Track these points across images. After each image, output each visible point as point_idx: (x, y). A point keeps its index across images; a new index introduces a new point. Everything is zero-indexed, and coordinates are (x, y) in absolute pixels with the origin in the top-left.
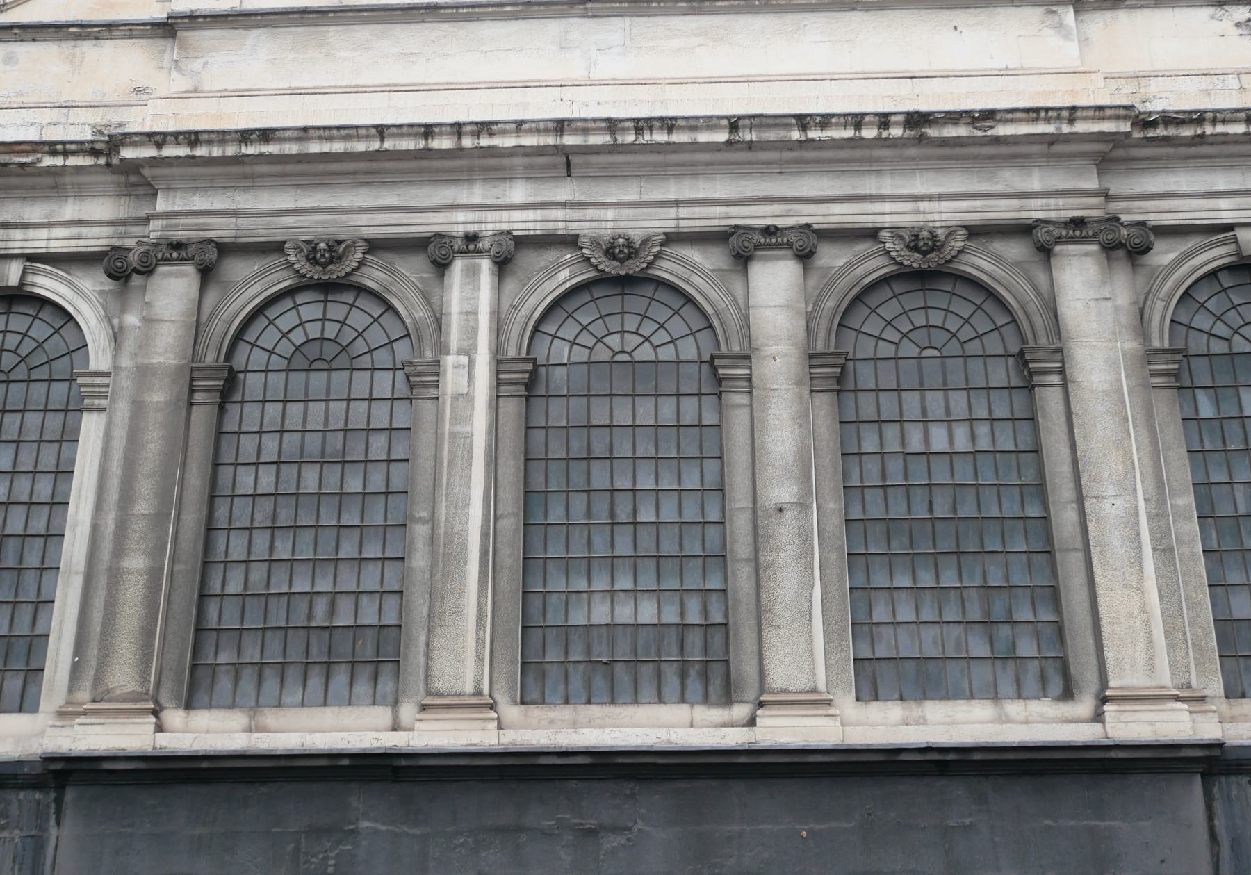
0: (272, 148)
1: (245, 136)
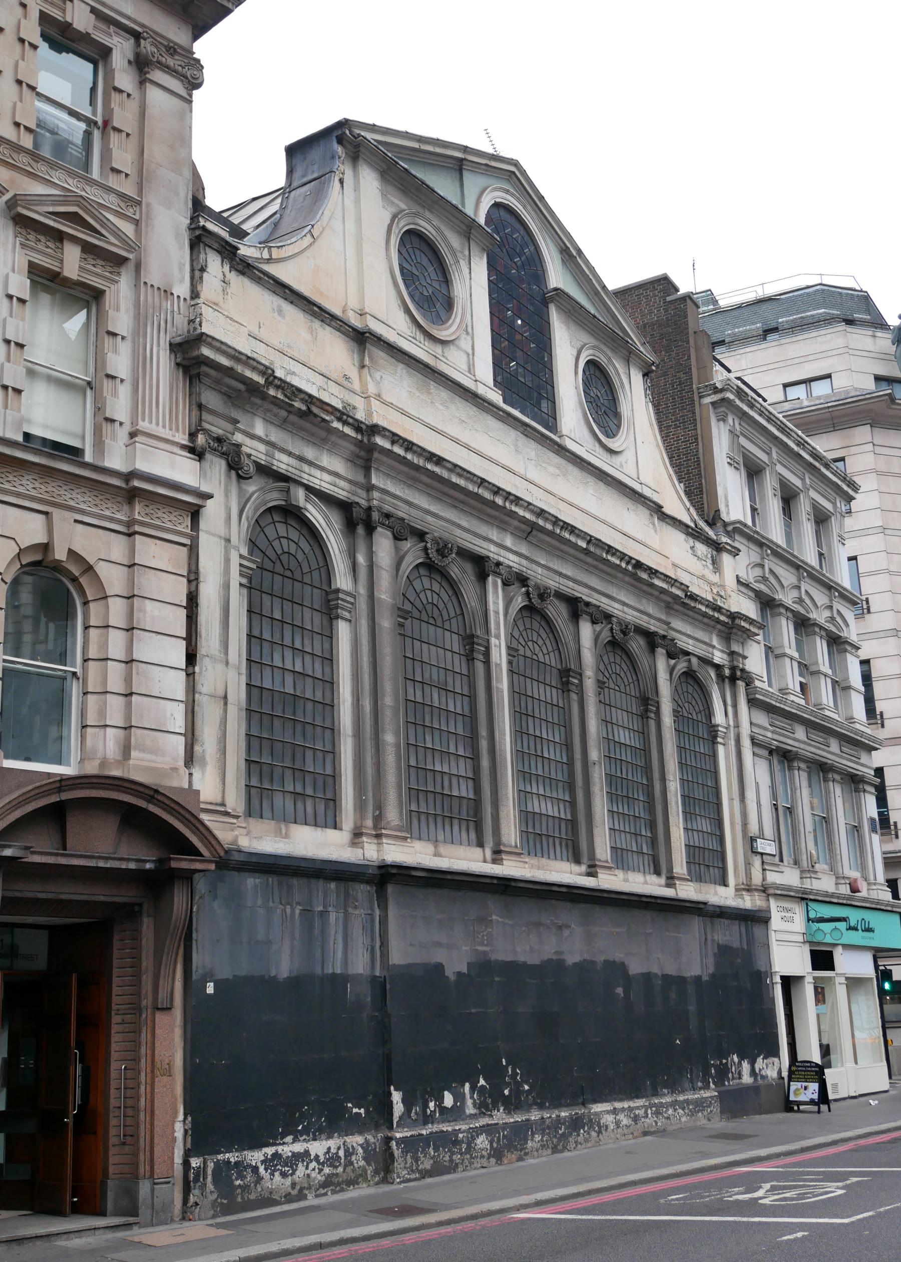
0: (437, 470)
1: (566, 526)
